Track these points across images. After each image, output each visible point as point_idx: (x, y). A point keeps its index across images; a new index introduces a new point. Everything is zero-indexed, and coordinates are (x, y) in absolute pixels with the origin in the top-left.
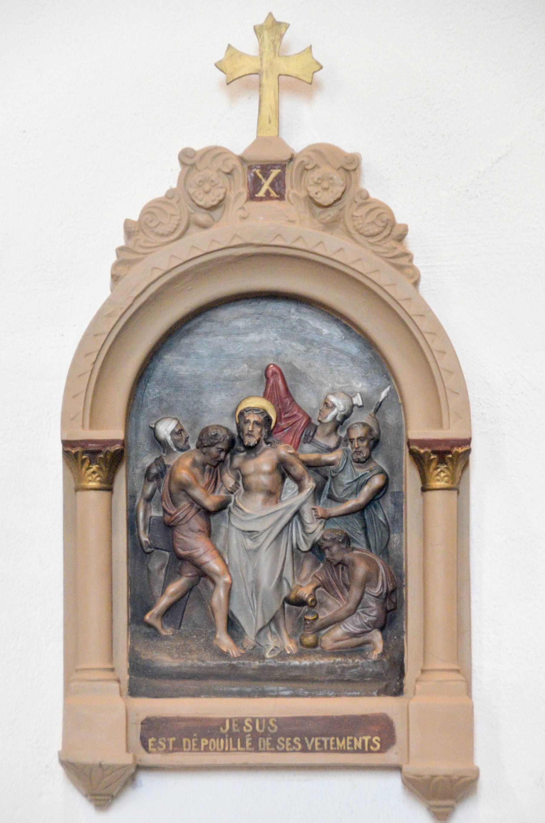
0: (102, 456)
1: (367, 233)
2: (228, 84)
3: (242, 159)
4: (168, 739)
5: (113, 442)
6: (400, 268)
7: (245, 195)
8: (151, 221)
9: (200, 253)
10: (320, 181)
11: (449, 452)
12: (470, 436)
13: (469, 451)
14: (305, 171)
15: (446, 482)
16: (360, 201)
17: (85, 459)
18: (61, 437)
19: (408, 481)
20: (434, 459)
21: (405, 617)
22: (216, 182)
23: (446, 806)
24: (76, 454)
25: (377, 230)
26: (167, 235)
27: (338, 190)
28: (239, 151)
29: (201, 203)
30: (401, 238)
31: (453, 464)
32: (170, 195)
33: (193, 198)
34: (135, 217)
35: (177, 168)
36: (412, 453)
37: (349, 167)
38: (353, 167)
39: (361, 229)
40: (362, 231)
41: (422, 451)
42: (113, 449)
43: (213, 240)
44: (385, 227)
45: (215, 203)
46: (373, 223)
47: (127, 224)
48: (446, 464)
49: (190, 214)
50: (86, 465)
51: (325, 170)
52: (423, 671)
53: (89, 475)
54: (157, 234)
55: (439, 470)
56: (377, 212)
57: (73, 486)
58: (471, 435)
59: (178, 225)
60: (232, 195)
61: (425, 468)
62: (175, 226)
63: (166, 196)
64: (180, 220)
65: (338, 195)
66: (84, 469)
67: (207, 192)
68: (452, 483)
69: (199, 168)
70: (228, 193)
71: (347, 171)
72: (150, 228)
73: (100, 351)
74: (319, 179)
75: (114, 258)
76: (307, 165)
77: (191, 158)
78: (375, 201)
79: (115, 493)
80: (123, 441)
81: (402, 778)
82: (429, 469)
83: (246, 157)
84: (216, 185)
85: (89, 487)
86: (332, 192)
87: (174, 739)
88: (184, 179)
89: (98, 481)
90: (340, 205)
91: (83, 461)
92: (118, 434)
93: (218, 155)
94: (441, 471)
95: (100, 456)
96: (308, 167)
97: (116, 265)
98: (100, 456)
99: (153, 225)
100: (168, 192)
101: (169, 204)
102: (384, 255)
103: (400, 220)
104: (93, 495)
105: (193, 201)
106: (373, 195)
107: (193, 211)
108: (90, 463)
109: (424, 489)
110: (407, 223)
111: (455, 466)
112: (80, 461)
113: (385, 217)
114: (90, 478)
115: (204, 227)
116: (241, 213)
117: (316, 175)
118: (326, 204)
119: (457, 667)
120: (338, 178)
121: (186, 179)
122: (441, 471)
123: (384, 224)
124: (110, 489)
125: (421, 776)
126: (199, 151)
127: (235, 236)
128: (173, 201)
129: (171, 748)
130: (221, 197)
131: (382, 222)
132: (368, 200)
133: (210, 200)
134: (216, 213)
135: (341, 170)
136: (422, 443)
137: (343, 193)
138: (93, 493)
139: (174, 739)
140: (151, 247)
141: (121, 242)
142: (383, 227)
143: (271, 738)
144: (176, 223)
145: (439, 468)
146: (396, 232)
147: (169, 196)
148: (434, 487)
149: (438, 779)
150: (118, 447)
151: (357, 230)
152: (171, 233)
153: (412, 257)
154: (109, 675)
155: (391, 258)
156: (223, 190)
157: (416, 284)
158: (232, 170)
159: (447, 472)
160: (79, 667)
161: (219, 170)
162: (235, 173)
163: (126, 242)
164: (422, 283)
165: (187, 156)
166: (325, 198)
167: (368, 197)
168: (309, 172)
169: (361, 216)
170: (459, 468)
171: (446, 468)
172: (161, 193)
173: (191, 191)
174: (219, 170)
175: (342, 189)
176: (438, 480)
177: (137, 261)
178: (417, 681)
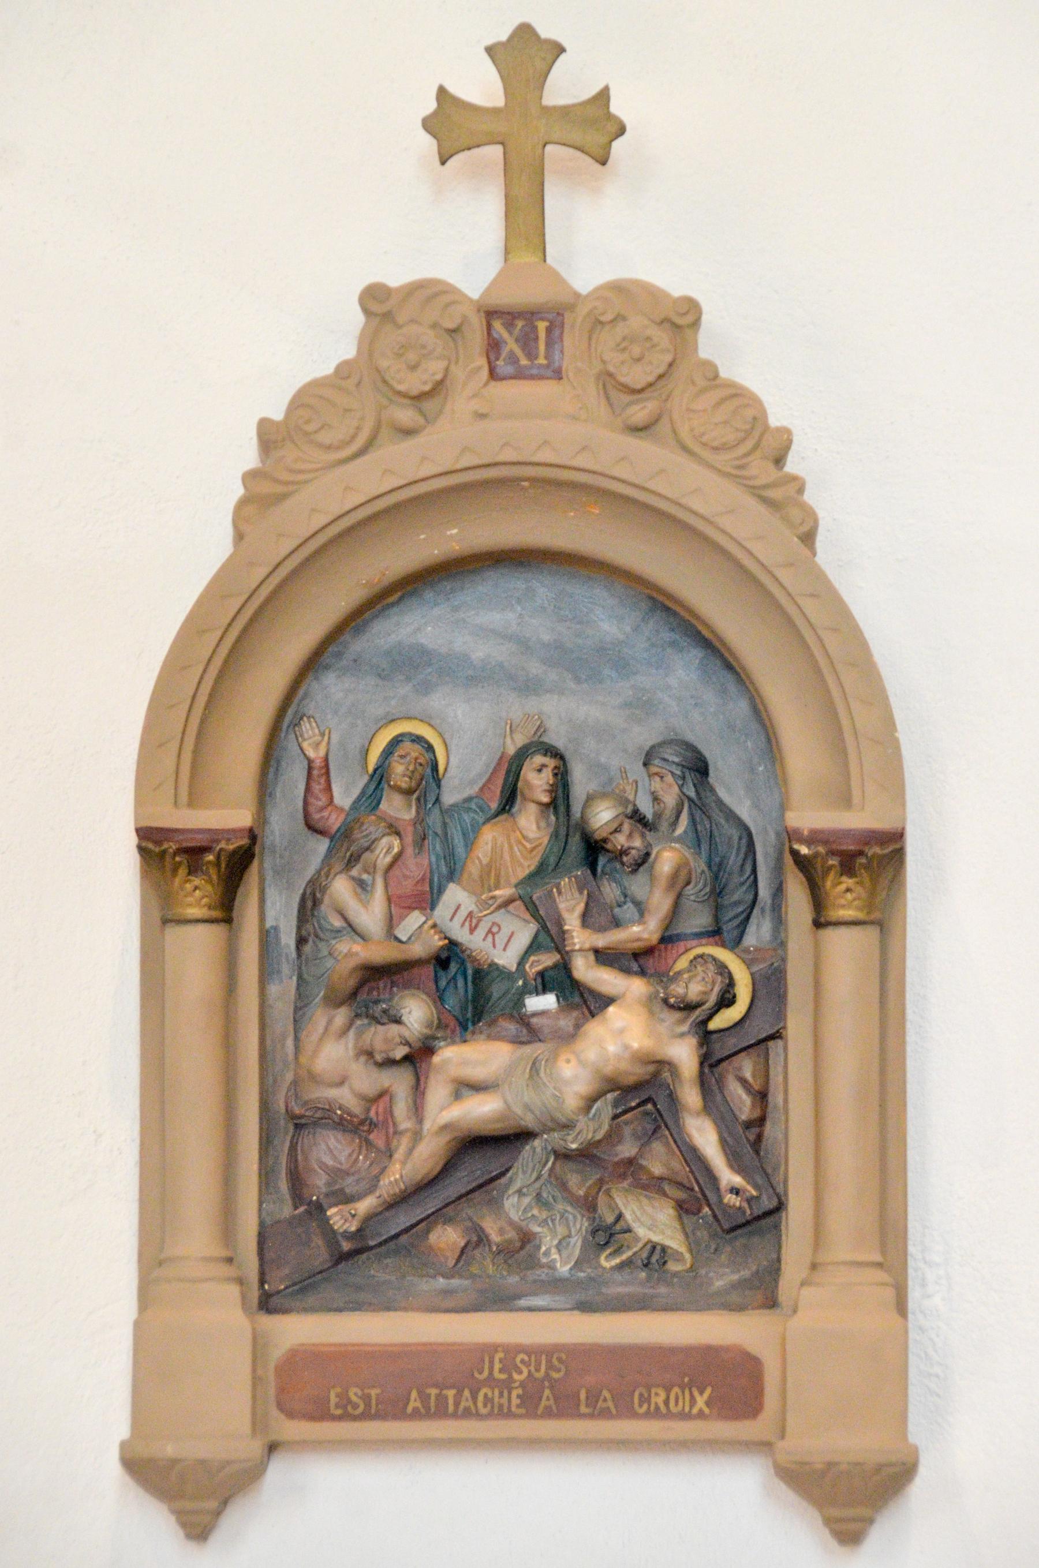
1: (715, 444)
4: (445, 1392)
5: (230, 833)
7: (485, 373)
9: (362, 499)
11: (861, 853)
12: (900, 826)
14: (599, 327)
16: (701, 383)
17: (180, 863)
18: (136, 820)
21: (343, 1349)
23: (854, 1520)
25: (731, 437)
26: (338, 448)
27: (660, 361)
29: (401, 388)
30: (779, 461)
32: (344, 370)
33: (388, 378)
34: (277, 414)
35: (360, 318)
37: (679, 321)
38: (689, 319)
40: (704, 439)
43: (313, 510)
44: (748, 433)
51: (636, 322)
56: (735, 402)
57: (156, 915)
59: (358, 428)
60: (458, 373)
64: (362, 418)
65: (661, 370)
66: (177, 881)
67: (413, 368)
68: (868, 913)
69: (401, 319)
70: (453, 368)
71: (677, 327)
72: (306, 434)
73: (209, 660)
75: (239, 491)
76: (603, 314)
77: (382, 302)
78: (731, 385)
80: (251, 830)
81: (465, 296)
85: (190, 917)
86: (651, 363)
88: (368, 341)
91: (175, 870)
92: (242, 818)
93: (736, 395)
96: (602, 319)
97: (242, 504)
100: (339, 368)
101: (341, 389)
102: (745, 482)
103: (774, 421)
106: (723, 374)
109: (818, 924)
111: (875, 881)
113: (749, 413)
114: (842, 901)
115: (408, 432)
116: (475, 405)
118: (639, 387)
120: (662, 337)
121: (372, 343)
123: (748, 427)
124: (228, 920)
125: (806, 1464)
126: (399, 289)
127: (465, 450)
128: (350, 384)
130: (439, 377)
132: (717, 382)
133: (415, 383)
134: (430, 406)
135: (667, 325)
136: (814, 838)
137: (671, 365)
139: (378, 1391)
140: (310, 471)
141: (249, 457)
142: (746, 431)
143: (520, 1391)
145: (841, 883)
148: (834, 919)
150: (245, 841)
154: (225, 1270)
156: (442, 364)
157: (808, 538)
158: (461, 325)
159: (859, 889)
160: (162, 1256)
161: (434, 326)
165: (374, 298)
166: (637, 376)
167: (716, 376)
168: (607, 328)
170: (884, 882)
173: (384, 364)
174: (434, 326)
175: (668, 358)
177: (283, 497)
178: (803, 1284)
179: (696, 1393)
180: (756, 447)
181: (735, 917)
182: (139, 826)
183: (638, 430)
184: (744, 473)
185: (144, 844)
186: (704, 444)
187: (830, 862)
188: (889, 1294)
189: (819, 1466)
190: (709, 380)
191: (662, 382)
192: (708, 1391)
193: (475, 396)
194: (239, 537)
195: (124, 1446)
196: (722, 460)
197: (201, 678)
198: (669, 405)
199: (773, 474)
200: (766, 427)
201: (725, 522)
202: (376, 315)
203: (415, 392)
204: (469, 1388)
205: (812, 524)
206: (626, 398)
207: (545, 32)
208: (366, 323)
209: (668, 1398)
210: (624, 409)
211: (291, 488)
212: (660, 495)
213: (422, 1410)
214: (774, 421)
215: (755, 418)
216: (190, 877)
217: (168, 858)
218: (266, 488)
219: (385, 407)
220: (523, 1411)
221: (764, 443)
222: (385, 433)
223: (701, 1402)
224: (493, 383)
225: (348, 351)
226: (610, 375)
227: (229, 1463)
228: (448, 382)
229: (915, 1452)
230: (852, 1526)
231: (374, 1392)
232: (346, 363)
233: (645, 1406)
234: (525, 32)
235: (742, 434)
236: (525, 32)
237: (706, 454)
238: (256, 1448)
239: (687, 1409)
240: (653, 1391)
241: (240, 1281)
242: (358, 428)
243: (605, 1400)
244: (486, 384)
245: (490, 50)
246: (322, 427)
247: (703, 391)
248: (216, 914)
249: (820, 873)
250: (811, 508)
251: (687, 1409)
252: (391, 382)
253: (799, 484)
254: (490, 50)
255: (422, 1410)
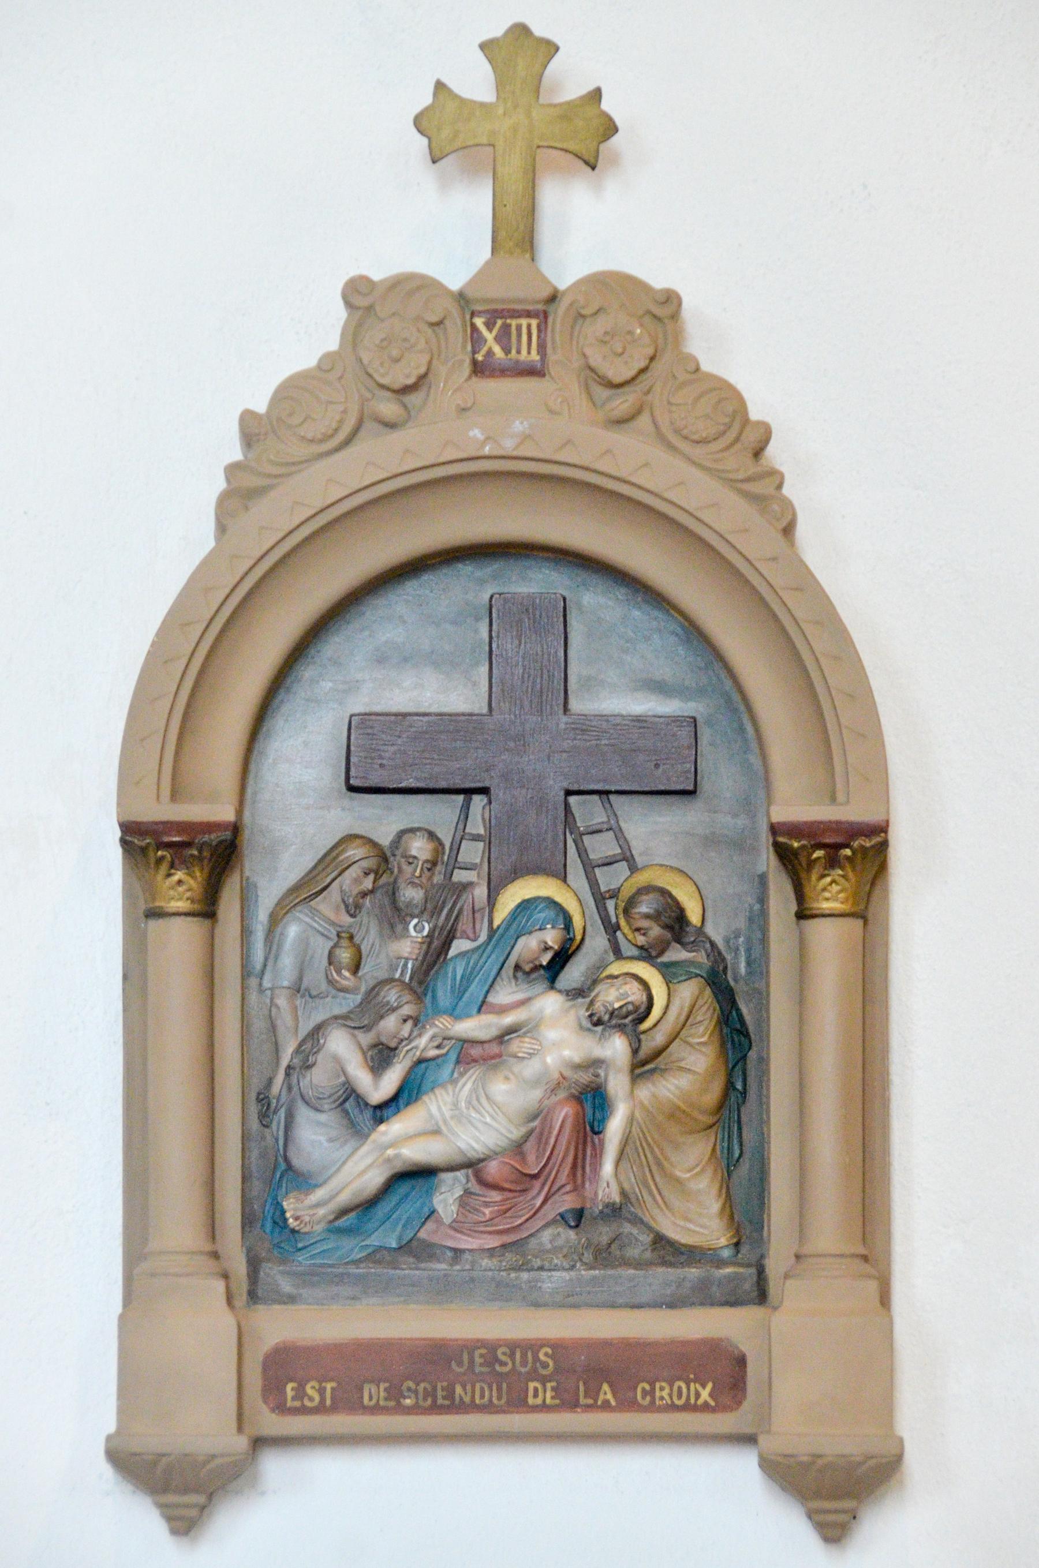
0: (196, 853)
1: (696, 437)
2: (434, 162)
3: (461, 298)
4: (324, 1384)
6: (759, 500)
8: (291, 415)
10: (607, 338)
13: (884, 845)
14: (580, 321)
15: (842, 903)
16: (682, 377)
17: (163, 858)
19: (771, 897)
20: (818, 858)
22: (413, 340)
24: (144, 850)
26: (321, 441)
28: (455, 284)
30: (758, 453)
31: (854, 870)
32: (328, 363)
33: (371, 371)
34: (261, 406)
35: (339, 314)
36: (776, 845)
37: (658, 311)
39: (686, 427)
40: (685, 432)
41: (796, 845)
42: (214, 838)
45: (410, 381)
46: (707, 417)
47: (247, 419)
48: (842, 868)
49: (363, 401)
50: (164, 868)
52: (798, 1257)
53: (172, 888)
54: (303, 438)
55: (828, 879)
58: (888, 812)
59: (341, 422)
61: (803, 875)
62: (334, 425)
63: (319, 367)
64: (345, 412)
65: (643, 364)
70: (435, 362)
73: (193, 654)
74: (606, 333)
75: (220, 484)
76: (583, 307)
79: (220, 922)
82: (809, 880)
83: (470, 294)
84: (412, 347)
85: (170, 910)
87: (334, 1384)
88: (353, 334)
89: (188, 899)
90: (645, 380)
91: (160, 861)
94: (833, 881)
95: (190, 852)
96: (584, 312)
98: (190, 852)
99: (296, 420)
102: (723, 475)
103: (755, 414)
104: (178, 924)
105: (370, 376)
106: (706, 367)
107: (368, 395)
108: (172, 866)
109: (802, 915)
110: (768, 419)
112: (152, 861)
115: (391, 426)
117: (598, 327)
118: (618, 380)
119: (864, 1252)
122: (833, 881)
123: (727, 420)
125: (792, 1456)
126: (382, 282)
129: (328, 1402)
130: (422, 370)
131: (726, 416)
134: (414, 399)
135: (647, 319)
136: (795, 830)
138: (178, 921)
139: (334, 1384)
142: (725, 424)
144: (338, 418)
145: (828, 875)
146: (751, 437)
147: (325, 367)
149: (825, 1460)
150: (228, 835)
151: (677, 431)
152: (326, 438)
153: (782, 476)
155: (742, 481)
157: (788, 530)
158: (444, 318)
162: (447, 322)
163: (245, 457)
164: (802, 531)
166: (619, 372)
167: (697, 369)
169: (686, 404)
171: (843, 876)
172: (308, 361)
174: (418, 318)
175: (650, 351)
176: (827, 899)
178: (786, 1276)
179: (700, 1389)
180: (737, 440)
181: (439, 347)
182: (121, 820)
183: (620, 422)
184: (721, 467)
185: (128, 838)
186: (686, 438)
187: (815, 856)
188: (873, 1286)
189: (805, 1459)
190: (691, 373)
191: (643, 377)
192: (710, 1386)
193: (459, 389)
194: (222, 529)
195: (109, 1438)
196: (698, 452)
197: (184, 672)
198: (650, 397)
199: (752, 470)
200: (746, 421)
201: (706, 516)
202: (358, 308)
203: (397, 386)
204: (608, 1382)
205: (790, 517)
206: (605, 393)
207: (539, 30)
208: (349, 315)
209: (671, 1390)
210: (604, 404)
211: (276, 481)
212: (640, 487)
213: (713, 1403)
214: (754, 415)
215: (735, 411)
216: (173, 871)
217: (151, 854)
218: (253, 481)
219: (368, 400)
220: (557, 1401)
221: (743, 438)
222: (369, 425)
223: (705, 1394)
224: (474, 379)
225: (333, 344)
226: (592, 369)
227: (214, 1457)
228: (430, 376)
229: (901, 1441)
230: (841, 1518)
231: (329, 1386)
232: (327, 356)
233: (648, 1398)
234: (521, 31)
235: (722, 428)
236: (521, 31)
237: (682, 445)
238: (242, 1443)
239: (692, 1401)
240: (658, 1385)
241: (226, 1276)
242: (341, 422)
243: (605, 1393)
244: (470, 377)
245: (485, 47)
246: (305, 420)
247: (684, 384)
248: (196, 907)
249: (804, 864)
250: (788, 499)
251: (692, 1401)
252: (376, 376)
253: (777, 478)
254: (485, 47)
255: (613, 1403)
